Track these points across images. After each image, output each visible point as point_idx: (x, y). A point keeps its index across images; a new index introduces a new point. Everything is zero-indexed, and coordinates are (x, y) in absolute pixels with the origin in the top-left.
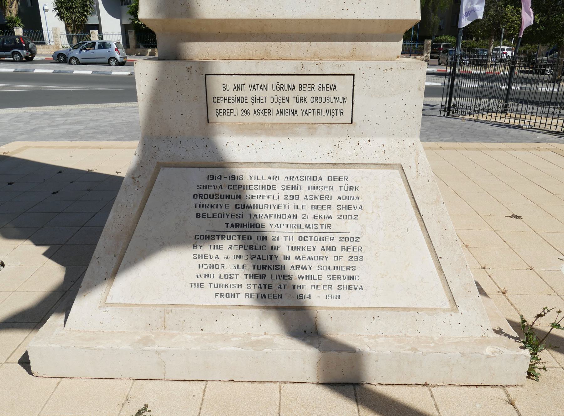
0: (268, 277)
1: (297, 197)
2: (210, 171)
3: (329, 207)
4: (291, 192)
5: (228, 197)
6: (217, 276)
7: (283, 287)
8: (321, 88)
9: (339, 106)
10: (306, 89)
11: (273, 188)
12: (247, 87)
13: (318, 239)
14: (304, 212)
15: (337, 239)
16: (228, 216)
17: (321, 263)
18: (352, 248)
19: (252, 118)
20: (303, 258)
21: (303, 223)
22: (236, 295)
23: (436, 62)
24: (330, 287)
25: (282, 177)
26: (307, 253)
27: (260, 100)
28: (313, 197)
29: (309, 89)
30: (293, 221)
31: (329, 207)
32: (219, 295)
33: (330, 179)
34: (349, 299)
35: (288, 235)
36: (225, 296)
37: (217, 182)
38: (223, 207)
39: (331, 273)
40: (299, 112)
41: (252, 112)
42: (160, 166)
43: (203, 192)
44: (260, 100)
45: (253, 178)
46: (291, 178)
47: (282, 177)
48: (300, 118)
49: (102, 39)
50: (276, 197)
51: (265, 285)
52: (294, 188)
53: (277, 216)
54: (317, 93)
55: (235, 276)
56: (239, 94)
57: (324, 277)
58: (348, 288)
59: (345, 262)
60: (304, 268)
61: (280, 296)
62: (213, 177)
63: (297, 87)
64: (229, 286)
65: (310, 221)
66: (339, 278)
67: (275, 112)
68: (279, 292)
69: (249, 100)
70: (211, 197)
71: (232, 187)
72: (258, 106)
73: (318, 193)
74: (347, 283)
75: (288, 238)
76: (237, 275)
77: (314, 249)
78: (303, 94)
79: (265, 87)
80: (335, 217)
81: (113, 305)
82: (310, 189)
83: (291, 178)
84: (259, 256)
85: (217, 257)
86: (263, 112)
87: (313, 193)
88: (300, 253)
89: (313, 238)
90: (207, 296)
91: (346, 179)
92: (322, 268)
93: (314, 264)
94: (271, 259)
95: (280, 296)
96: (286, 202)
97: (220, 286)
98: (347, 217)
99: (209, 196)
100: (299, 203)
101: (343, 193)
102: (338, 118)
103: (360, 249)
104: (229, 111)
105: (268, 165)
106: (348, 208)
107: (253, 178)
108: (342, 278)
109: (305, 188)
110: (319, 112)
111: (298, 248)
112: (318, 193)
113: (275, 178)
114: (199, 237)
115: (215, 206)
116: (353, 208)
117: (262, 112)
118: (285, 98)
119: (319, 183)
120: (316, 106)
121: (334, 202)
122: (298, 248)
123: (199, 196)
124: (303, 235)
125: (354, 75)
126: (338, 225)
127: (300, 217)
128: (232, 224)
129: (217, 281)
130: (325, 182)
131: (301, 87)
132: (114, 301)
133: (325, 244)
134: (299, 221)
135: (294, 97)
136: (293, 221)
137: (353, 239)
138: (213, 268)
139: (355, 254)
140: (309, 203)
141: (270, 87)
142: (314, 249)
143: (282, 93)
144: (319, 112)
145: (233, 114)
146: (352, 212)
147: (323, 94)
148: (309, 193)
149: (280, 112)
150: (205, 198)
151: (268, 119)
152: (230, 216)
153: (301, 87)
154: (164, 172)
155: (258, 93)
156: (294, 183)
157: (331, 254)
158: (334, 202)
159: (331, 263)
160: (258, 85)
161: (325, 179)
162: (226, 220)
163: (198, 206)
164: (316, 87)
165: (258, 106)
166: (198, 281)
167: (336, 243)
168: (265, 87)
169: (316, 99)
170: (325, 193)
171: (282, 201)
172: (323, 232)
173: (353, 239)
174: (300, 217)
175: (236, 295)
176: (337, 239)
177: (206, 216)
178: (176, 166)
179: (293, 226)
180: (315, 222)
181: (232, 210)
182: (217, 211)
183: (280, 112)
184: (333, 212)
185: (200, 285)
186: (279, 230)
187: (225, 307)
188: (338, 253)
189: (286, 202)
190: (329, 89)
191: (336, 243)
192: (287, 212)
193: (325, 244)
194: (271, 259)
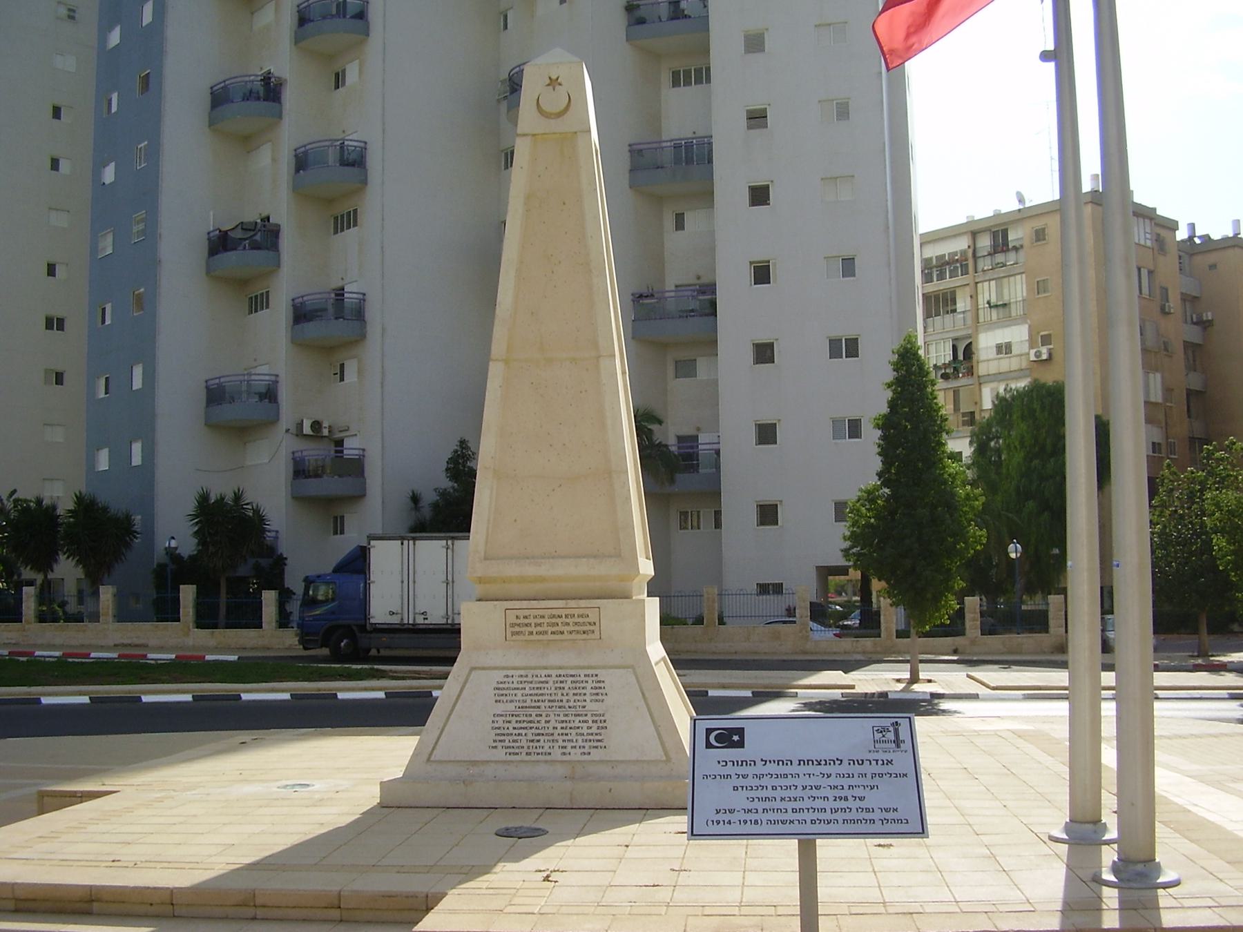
9: (592, 628)
17: (579, 731)
19: (535, 637)
27: (540, 625)
34: (596, 755)
37: (510, 680)
44: (540, 625)
56: (526, 621)
59: (594, 730)
62: (507, 676)
65: (571, 704)
72: (539, 629)
74: (596, 744)
79: (543, 617)
90: (500, 754)
93: (573, 732)
101: (595, 685)
102: (591, 636)
110: (578, 632)
120: (577, 628)
121: (588, 691)
126: (591, 706)
129: (507, 744)
130: (583, 678)
143: (554, 620)
144: (578, 632)
146: (600, 697)
147: (581, 620)
149: (553, 633)
158: (588, 691)
159: (585, 731)
165: (539, 629)
167: (589, 718)
168: (543, 617)
171: (553, 691)
178: (484, 669)
181: (519, 697)
182: (509, 698)
183: (553, 633)
184: (588, 698)
188: (590, 724)
191: (589, 718)
192: (506, 731)
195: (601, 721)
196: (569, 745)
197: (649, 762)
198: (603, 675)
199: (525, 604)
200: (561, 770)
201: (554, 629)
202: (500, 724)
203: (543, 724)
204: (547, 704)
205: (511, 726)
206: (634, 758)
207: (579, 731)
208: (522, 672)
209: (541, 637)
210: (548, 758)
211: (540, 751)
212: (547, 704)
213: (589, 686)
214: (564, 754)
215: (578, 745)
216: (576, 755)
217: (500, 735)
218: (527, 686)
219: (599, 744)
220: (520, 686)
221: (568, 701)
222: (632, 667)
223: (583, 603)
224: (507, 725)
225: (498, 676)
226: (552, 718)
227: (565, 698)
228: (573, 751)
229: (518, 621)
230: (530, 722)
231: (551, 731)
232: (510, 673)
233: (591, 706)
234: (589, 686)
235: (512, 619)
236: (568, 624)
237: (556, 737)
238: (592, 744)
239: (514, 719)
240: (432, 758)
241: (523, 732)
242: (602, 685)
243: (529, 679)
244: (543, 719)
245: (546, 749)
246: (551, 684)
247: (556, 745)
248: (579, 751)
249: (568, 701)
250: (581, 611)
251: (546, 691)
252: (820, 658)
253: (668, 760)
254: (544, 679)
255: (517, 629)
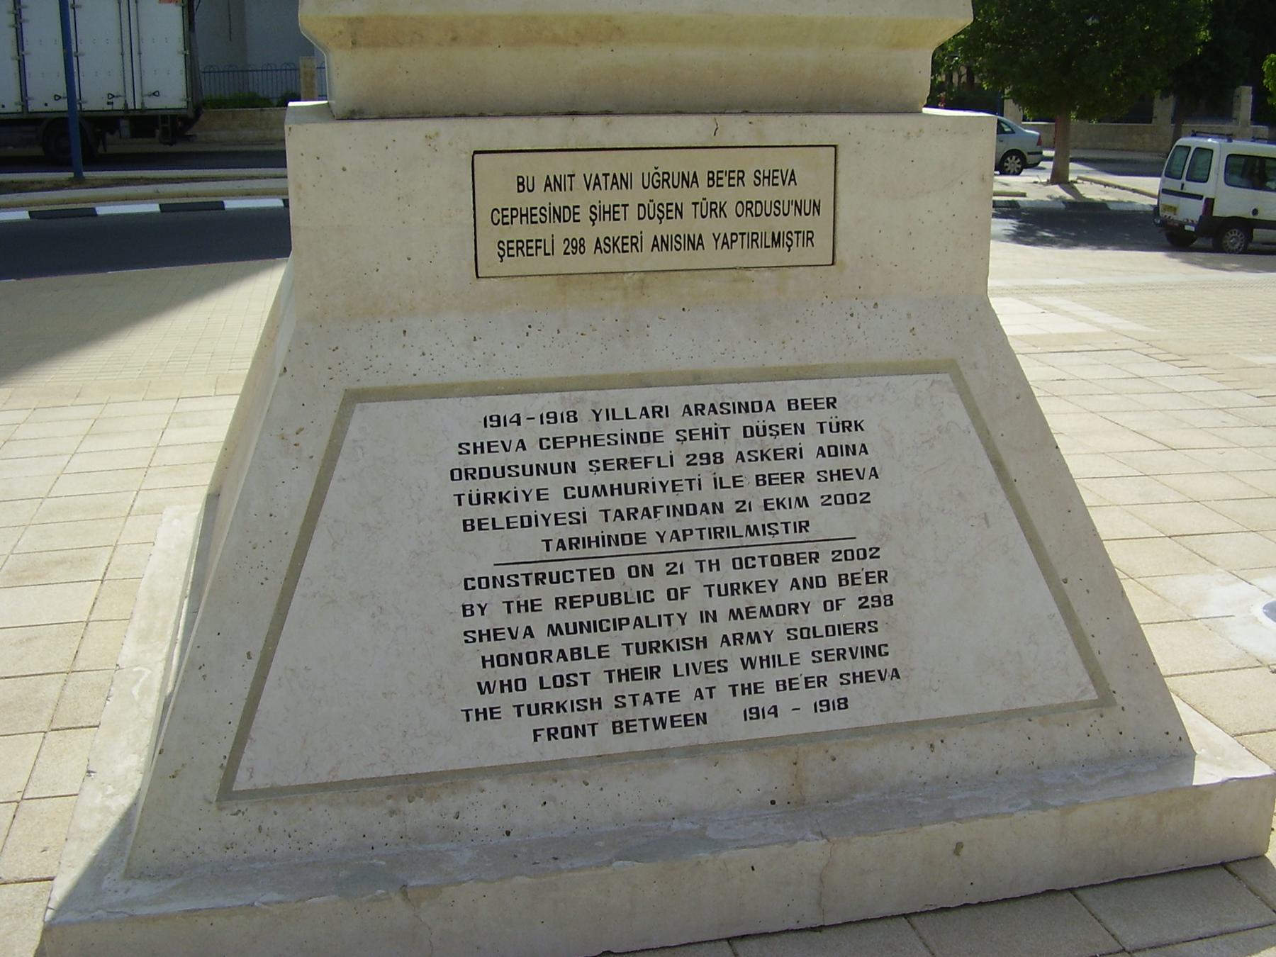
0: (667, 672)
1: (719, 458)
2: (490, 405)
3: (799, 478)
4: (699, 446)
5: (543, 470)
6: (533, 684)
7: (706, 693)
8: (760, 178)
10: (725, 182)
11: (653, 438)
12: (579, 182)
13: (777, 561)
14: (738, 494)
15: (826, 558)
16: (547, 521)
17: (796, 621)
18: (863, 575)
19: (590, 261)
20: (748, 613)
21: (740, 522)
22: (589, 730)
23: (1264, 130)
24: (822, 681)
25: (676, 409)
26: (758, 601)
27: (612, 213)
28: (758, 455)
29: (732, 182)
30: (716, 521)
31: (799, 478)
32: (544, 734)
33: (793, 407)
34: (870, 705)
35: (705, 556)
36: (559, 736)
37: (511, 434)
38: (533, 496)
39: (821, 644)
40: (708, 241)
41: (590, 245)
42: (355, 397)
43: (477, 461)
44: (612, 213)
45: (603, 416)
46: (700, 409)
47: (676, 409)
48: (710, 255)
49: (999, 122)
50: (665, 461)
51: (661, 694)
52: (708, 434)
53: (674, 511)
54: (749, 192)
55: (580, 679)
56: (558, 199)
57: (806, 658)
58: (866, 677)
59: (849, 613)
60: (754, 638)
61: (702, 719)
62: (499, 421)
63: (703, 180)
64: (568, 706)
65: (757, 517)
66: (841, 654)
67: (648, 242)
68: (698, 707)
69: (584, 214)
70: (499, 474)
71: (551, 443)
72: (607, 229)
73: (769, 443)
74: (861, 665)
75: (706, 565)
76: (585, 674)
77: (683, 620)
78: (716, 195)
79: (622, 181)
80: (814, 501)
81: (252, 794)
82: (749, 434)
83: (700, 409)
84: (638, 618)
85: (529, 632)
86: (619, 244)
87: (756, 443)
88: (740, 601)
89: (768, 560)
90: (512, 739)
91: (831, 403)
92: (798, 633)
93: (777, 625)
94: (670, 624)
95: (702, 719)
96: (692, 472)
97: (544, 708)
98: (845, 499)
99: (491, 473)
100: (726, 471)
101: (829, 439)
102: (800, 254)
103: (883, 576)
104: (533, 244)
105: (640, 381)
106: (843, 475)
107: (603, 416)
108: (848, 655)
109: (736, 433)
110: (754, 239)
111: (733, 589)
112: (769, 443)
113: (659, 411)
114: (476, 583)
115: (511, 497)
116: (855, 476)
117: (615, 244)
118: (673, 207)
119: (768, 418)
120: (750, 224)
121: (810, 464)
122: (733, 589)
123: (468, 474)
124: (743, 553)
125: (835, 146)
127: (729, 507)
128: (561, 541)
129: (534, 695)
130: (783, 415)
131: (713, 179)
132: (261, 781)
133: (799, 572)
134: (728, 518)
135: (695, 204)
136: (716, 521)
137: (863, 554)
138: (521, 663)
139: (871, 591)
140: (750, 470)
141: (637, 181)
142: (683, 620)
143: (664, 195)
144: (754, 239)
145: (541, 251)
146: (854, 486)
147: (766, 193)
148: (746, 445)
149: (661, 244)
150: (481, 477)
151: (631, 261)
152: (552, 521)
153: (713, 179)
154: (363, 420)
155: (608, 197)
156: (708, 421)
157: (813, 596)
158: (810, 464)
159: (818, 618)
160: (606, 175)
161: (781, 406)
162: (543, 531)
163: (465, 499)
164: (749, 178)
165: (607, 229)
166: (486, 702)
167: (826, 568)
168: (622, 181)
169: (748, 208)
170: (784, 442)
171: (681, 471)
172: (790, 542)
173: (863, 554)
174: (729, 507)
175: (589, 730)
176: (826, 558)
177: (490, 526)
179: (716, 533)
180: (769, 517)
181: (557, 504)
183: (661, 244)
184: (810, 489)
185: (491, 713)
186: (681, 545)
187: (563, 764)
188: (833, 590)
189: (692, 472)
190: (779, 181)
191: (826, 568)
192: (698, 498)
193: (799, 572)
194: (670, 624)
195: (865, 571)
196: (768, 676)
197: (1044, 713)
198: (855, 399)
199: (554, 130)
200: (752, 779)
201: (670, 228)
202: (497, 617)
203: (661, 605)
204: (667, 524)
205: (539, 622)
206: (997, 706)
207: (796, 621)
208: (552, 402)
209: (613, 261)
210: (697, 735)
211: (665, 710)
212: (667, 524)
213: (810, 443)
214: (755, 713)
215: (799, 672)
216: (797, 715)
217: (504, 665)
218: (582, 456)
219: (871, 662)
220: (554, 457)
221: (742, 507)
222: (951, 366)
223: (777, 128)
224: (520, 620)
225: (462, 420)
226: (692, 578)
227: (729, 497)
228: (784, 700)
229: (525, 201)
230: (613, 599)
231: (694, 628)
232: (507, 406)
233: (829, 522)
234: (810, 443)
235: (498, 188)
236: (717, 209)
237: (716, 651)
238: (849, 665)
239: (547, 593)
240: (242, 781)
241: (590, 641)
242: (854, 438)
243: (585, 427)
244: (659, 584)
245: (687, 704)
246: (669, 444)
247: (722, 682)
248: (806, 697)
249: (742, 507)
250: (769, 160)
251: (652, 474)
252: (244, 148)
253: (1105, 700)
254: (638, 425)
255: (521, 231)
